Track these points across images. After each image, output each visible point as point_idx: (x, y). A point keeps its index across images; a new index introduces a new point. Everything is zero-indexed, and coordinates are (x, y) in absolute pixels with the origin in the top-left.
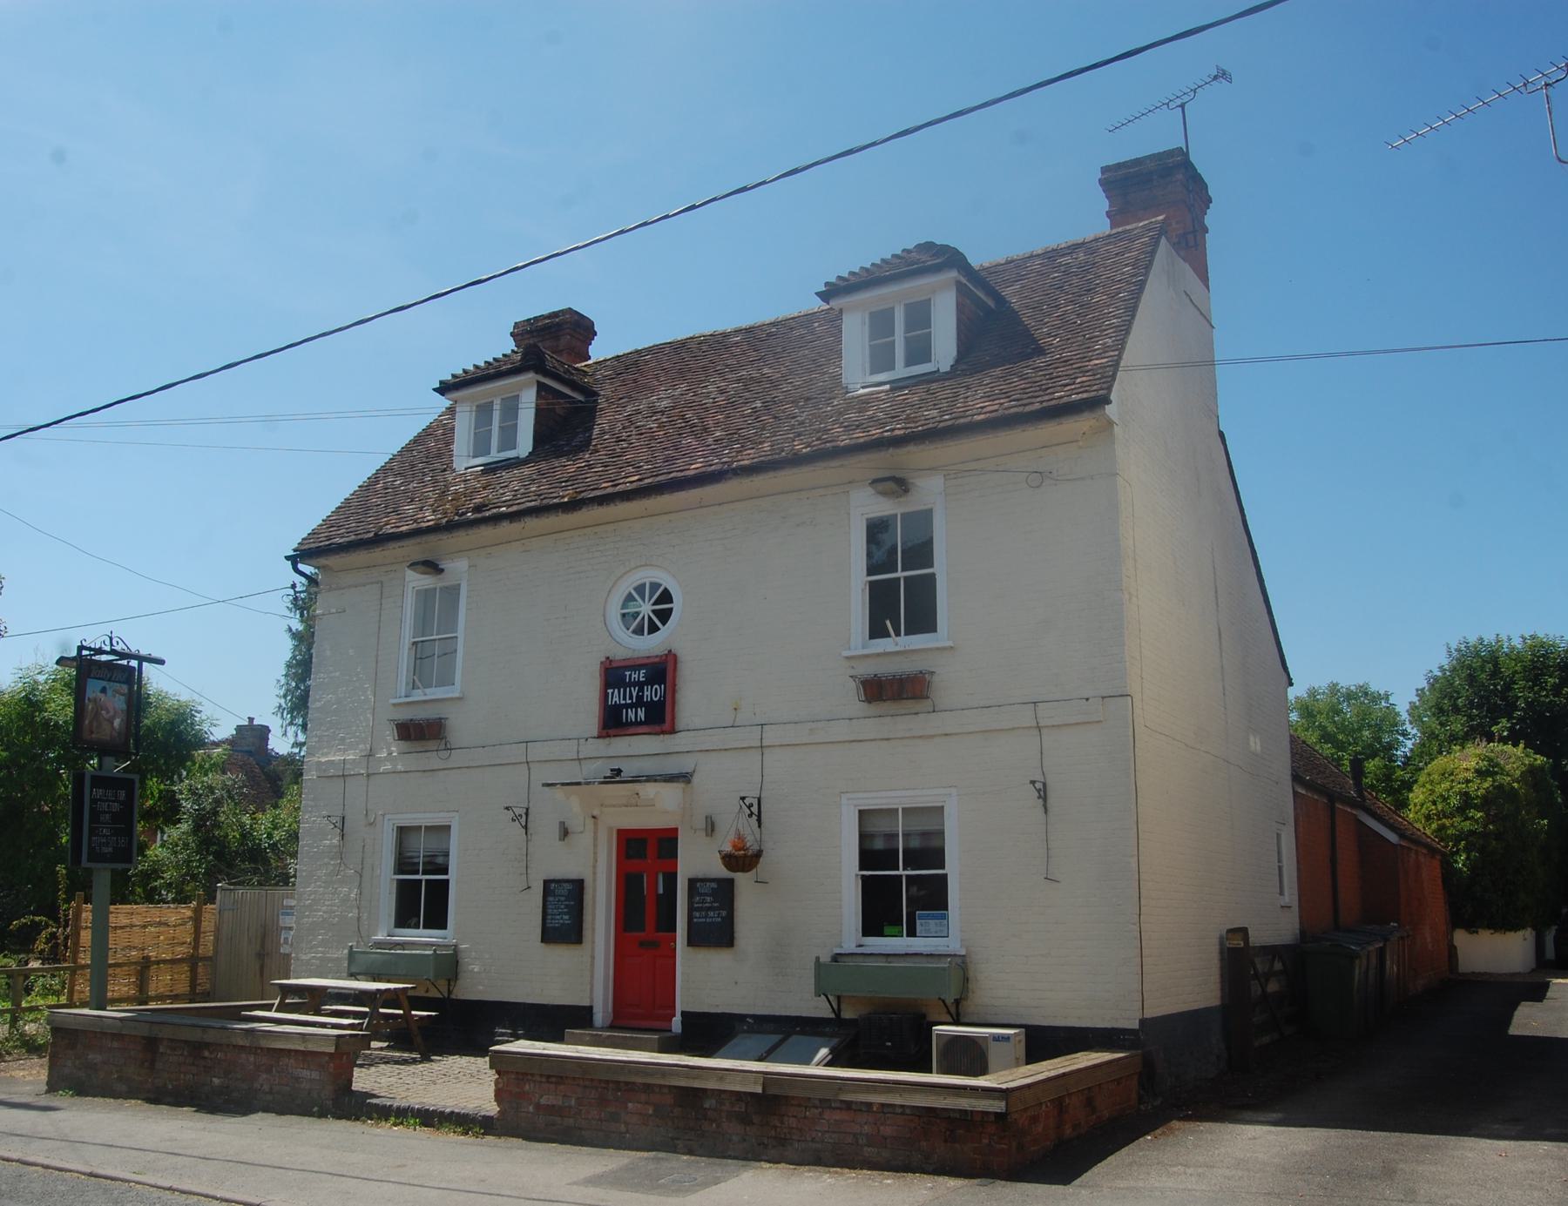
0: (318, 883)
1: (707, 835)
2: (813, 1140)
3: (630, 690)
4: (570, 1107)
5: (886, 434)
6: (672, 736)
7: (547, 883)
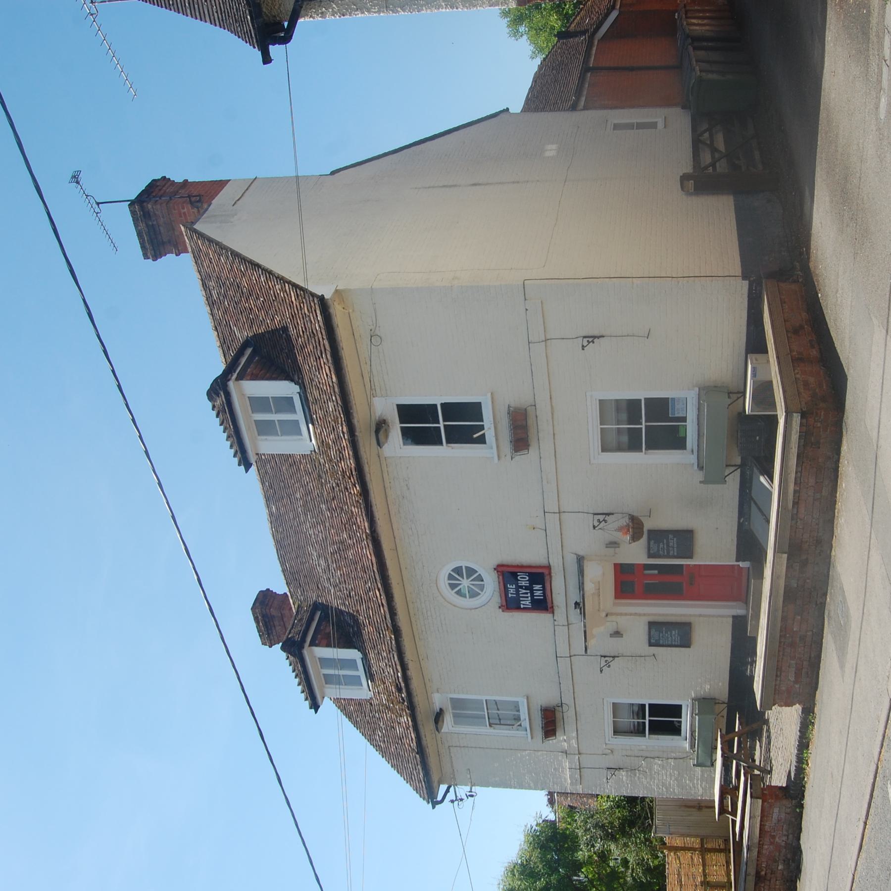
0: (652, 783)
1: (619, 547)
4: (796, 664)
5: (346, 437)
6: (552, 568)
7: (651, 645)
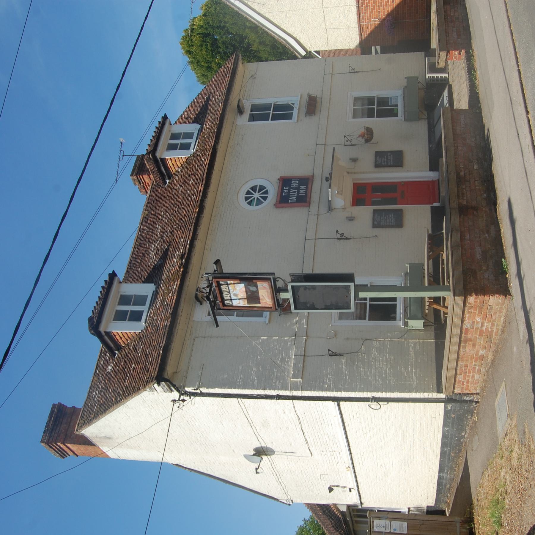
3: (291, 192)
6: (315, 177)
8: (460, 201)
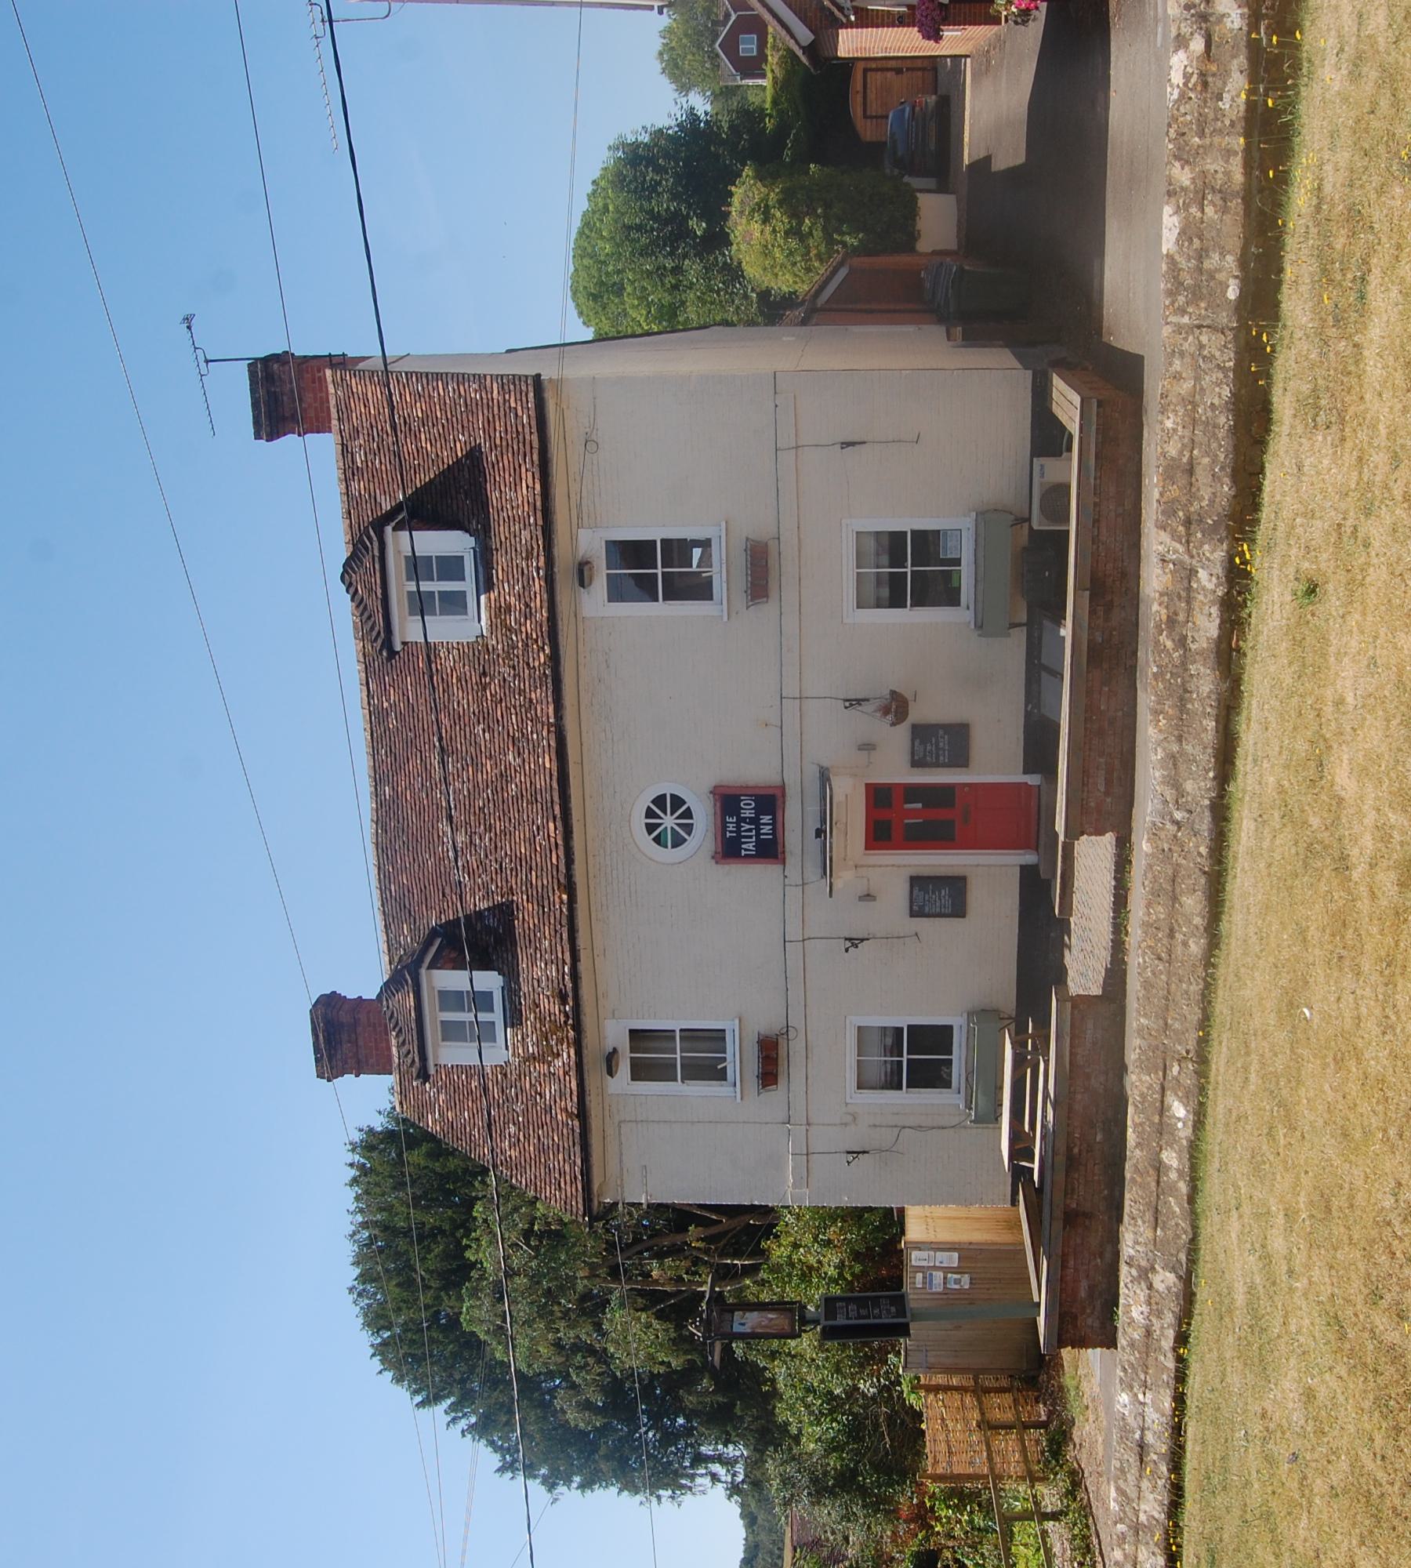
2: (1122, 550)
3: (745, 831)
6: (787, 790)
7: (913, 914)
8: (1068, 1201)
